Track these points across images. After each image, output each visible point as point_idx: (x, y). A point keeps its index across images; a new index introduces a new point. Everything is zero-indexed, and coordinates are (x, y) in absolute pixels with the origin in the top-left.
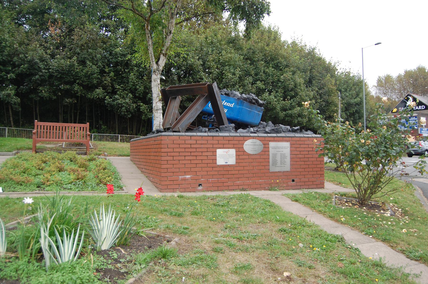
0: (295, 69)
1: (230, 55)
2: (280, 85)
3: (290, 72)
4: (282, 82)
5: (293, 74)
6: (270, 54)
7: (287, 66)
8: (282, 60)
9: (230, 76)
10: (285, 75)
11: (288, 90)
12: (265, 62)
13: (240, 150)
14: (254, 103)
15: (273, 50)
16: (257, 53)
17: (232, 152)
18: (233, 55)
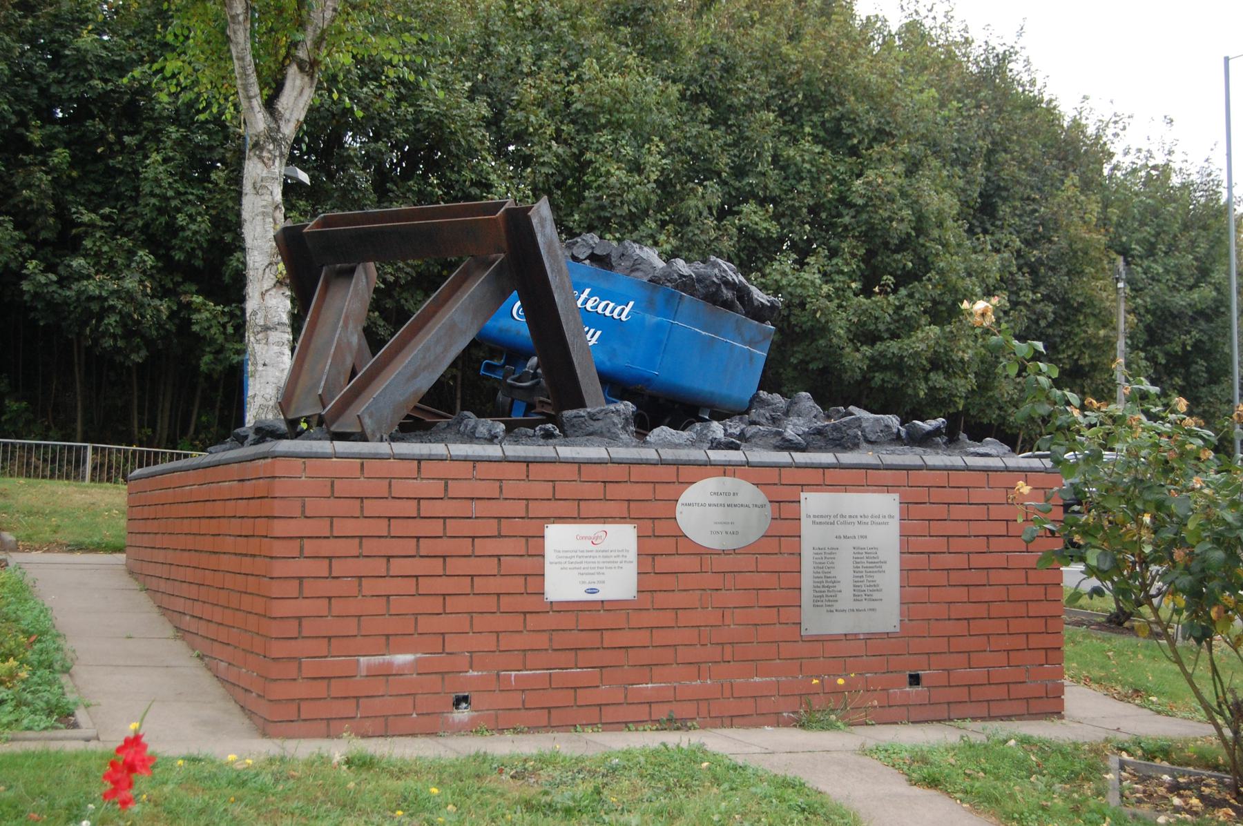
0: (918, 149)
1: (618, 80)
2: (847, 220)
3: (895, 160)
4: (860, 210)
5: (909, 173)
6: (804, 76)
7: (881, 135)
8: (861, 108)
9: (618, 174)
10: (871, 174)
11: (886, 244)
12: (782, 113)
13: (661, 527)
14: (727, 305)
15: (817, 57)
16: (742, 71)
17: (623, 537)
18: (631, 80)
